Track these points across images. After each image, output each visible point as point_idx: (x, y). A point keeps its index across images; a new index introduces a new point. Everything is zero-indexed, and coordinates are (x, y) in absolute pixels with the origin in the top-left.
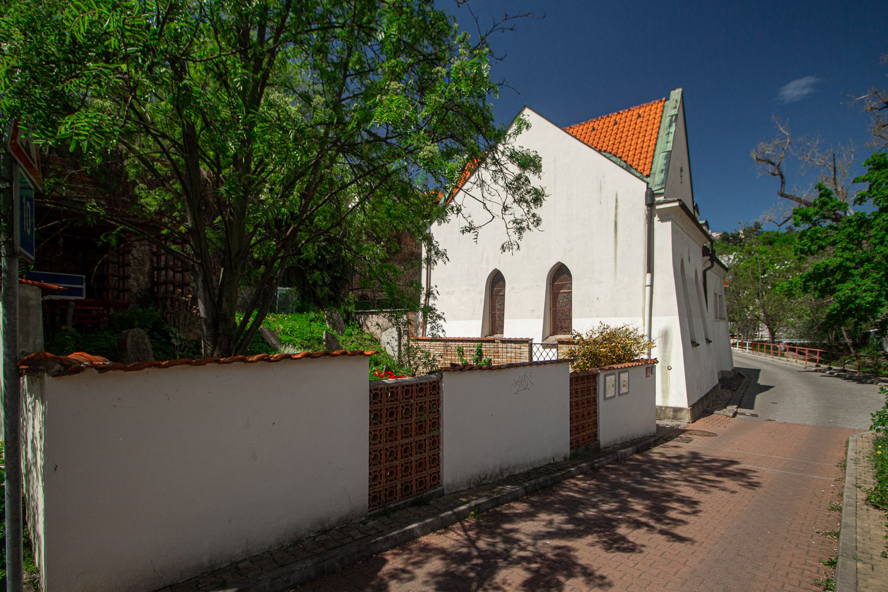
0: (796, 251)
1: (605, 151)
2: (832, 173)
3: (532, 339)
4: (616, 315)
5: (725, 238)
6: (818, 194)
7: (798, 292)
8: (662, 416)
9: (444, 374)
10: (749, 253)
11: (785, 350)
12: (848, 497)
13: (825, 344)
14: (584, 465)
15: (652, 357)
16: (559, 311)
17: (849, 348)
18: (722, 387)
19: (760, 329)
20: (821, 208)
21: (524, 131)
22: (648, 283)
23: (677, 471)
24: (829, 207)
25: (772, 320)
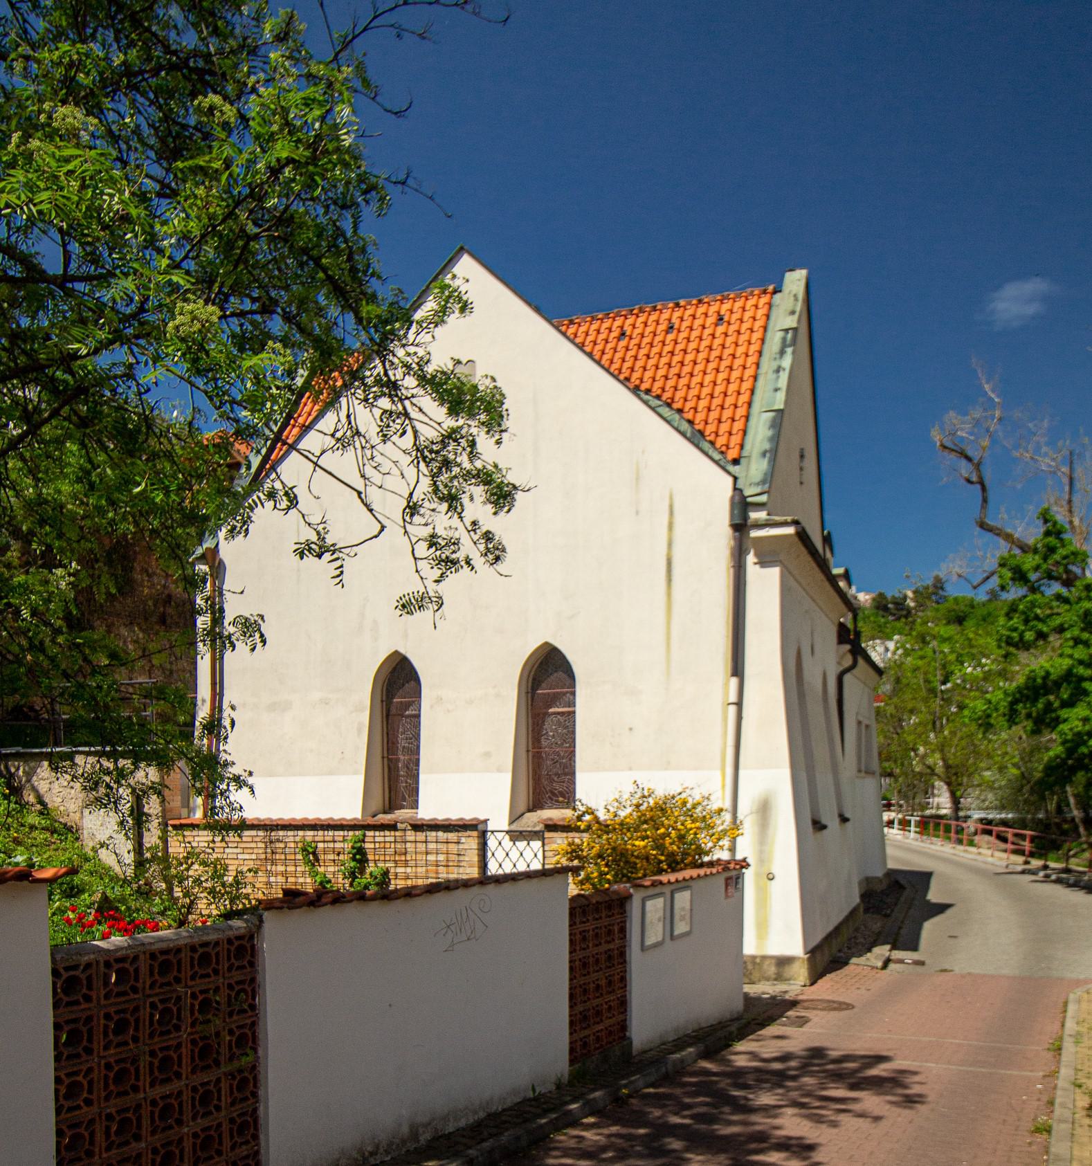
0: (999, 640)
1: (648, 391)
2: (1067, 488)
3: (486, 821)
4: (667, 766)
5: (881, 605)
6: (1042, 530)
7: (998, 720)
8: (756, 975)
9: (266, 915)
10: (923, 639)
11: (976, 833)
12: (1063, 1105)
13: (1040, 820)
14: (597, 1094)
15: (739, 856)
16: (548, 754)
17: (1076, 827)
18: (866, 910)
19: (936, 792)
20: (1045, 559)
21: (453, 319)
22: (733, 698)
23: (781, 1086)
24: (1057, 557)
25: (956, 774)
